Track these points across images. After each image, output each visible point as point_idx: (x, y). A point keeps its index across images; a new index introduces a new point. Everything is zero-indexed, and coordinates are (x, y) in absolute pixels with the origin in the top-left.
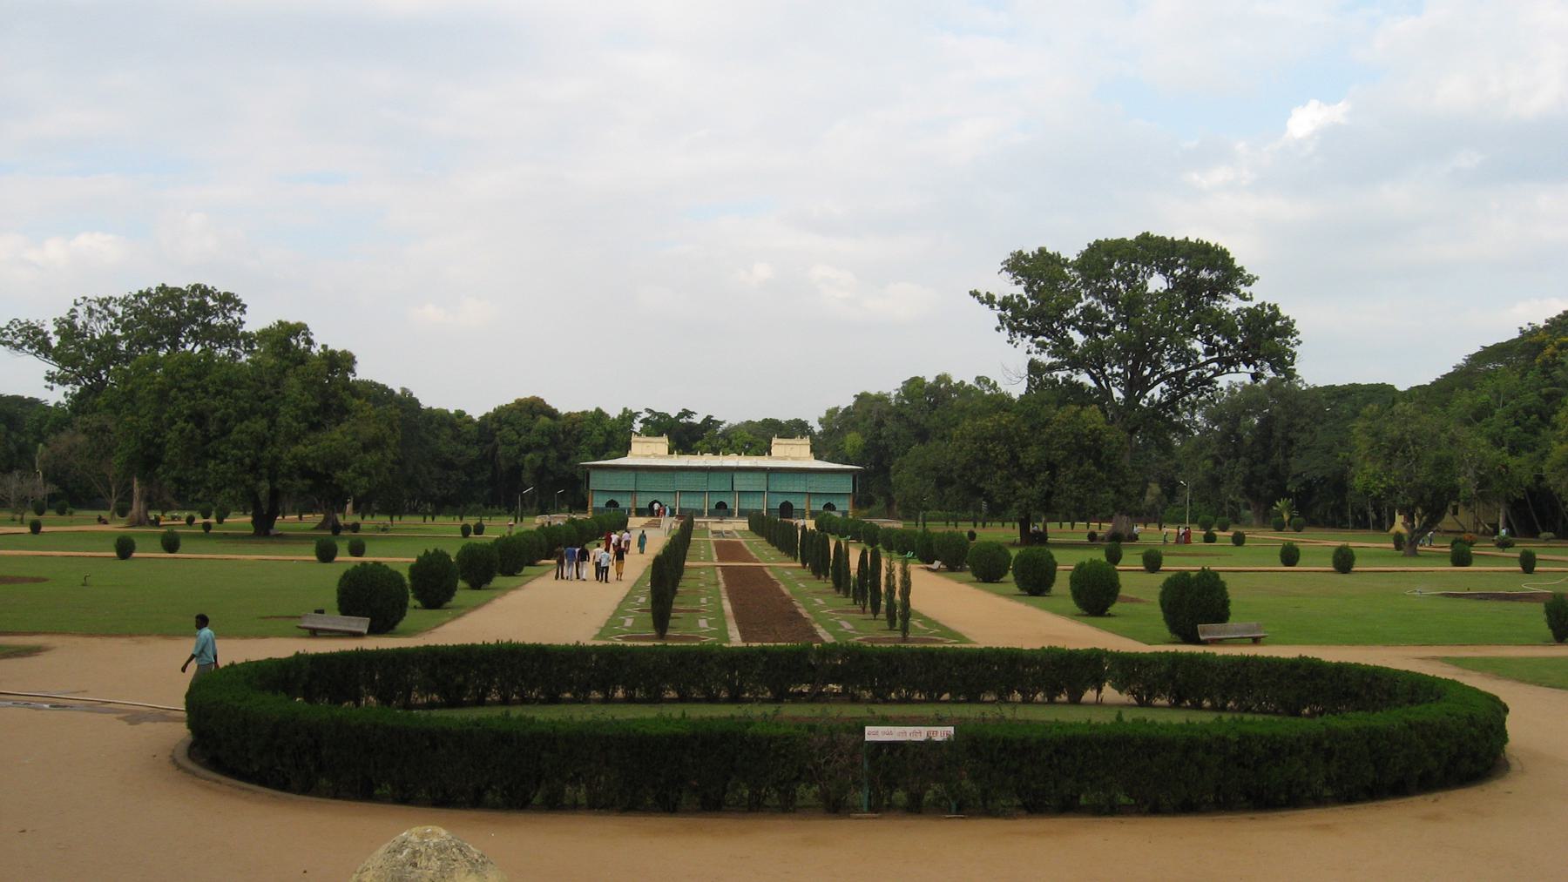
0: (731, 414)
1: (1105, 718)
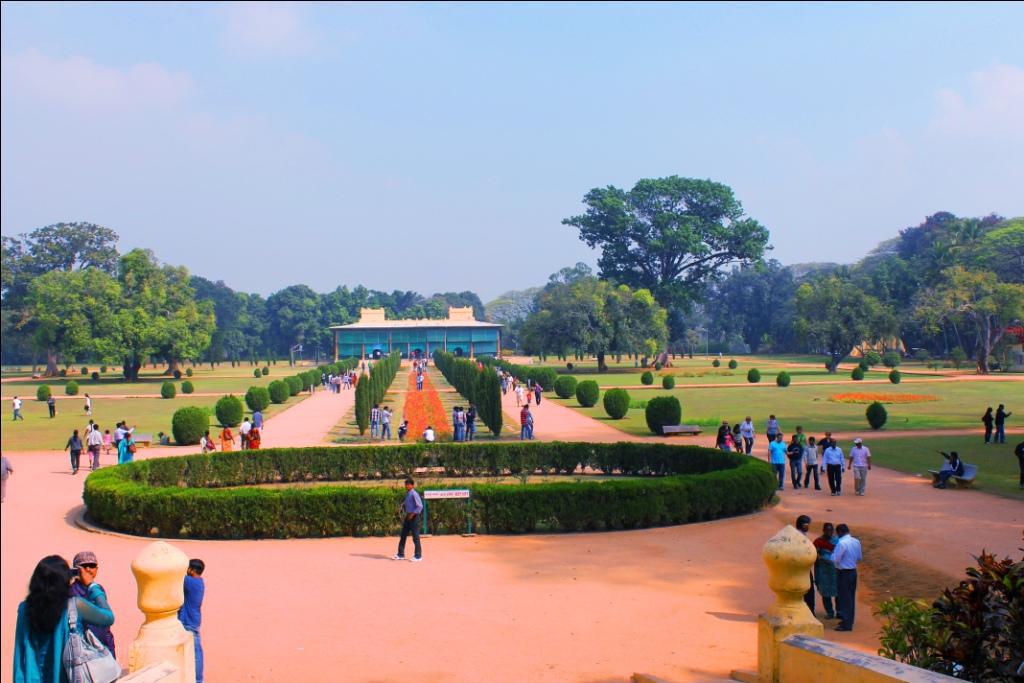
0: (425, 290)
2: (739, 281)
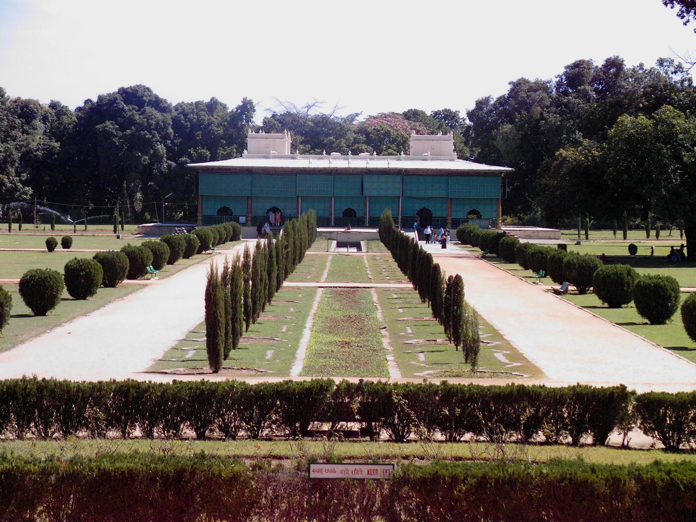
1: (622, 459)
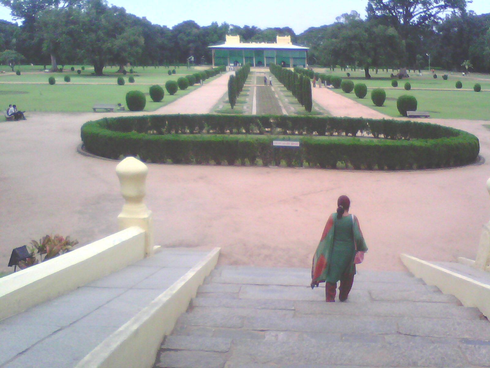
0: (262, 25)
2: (450, 23)
